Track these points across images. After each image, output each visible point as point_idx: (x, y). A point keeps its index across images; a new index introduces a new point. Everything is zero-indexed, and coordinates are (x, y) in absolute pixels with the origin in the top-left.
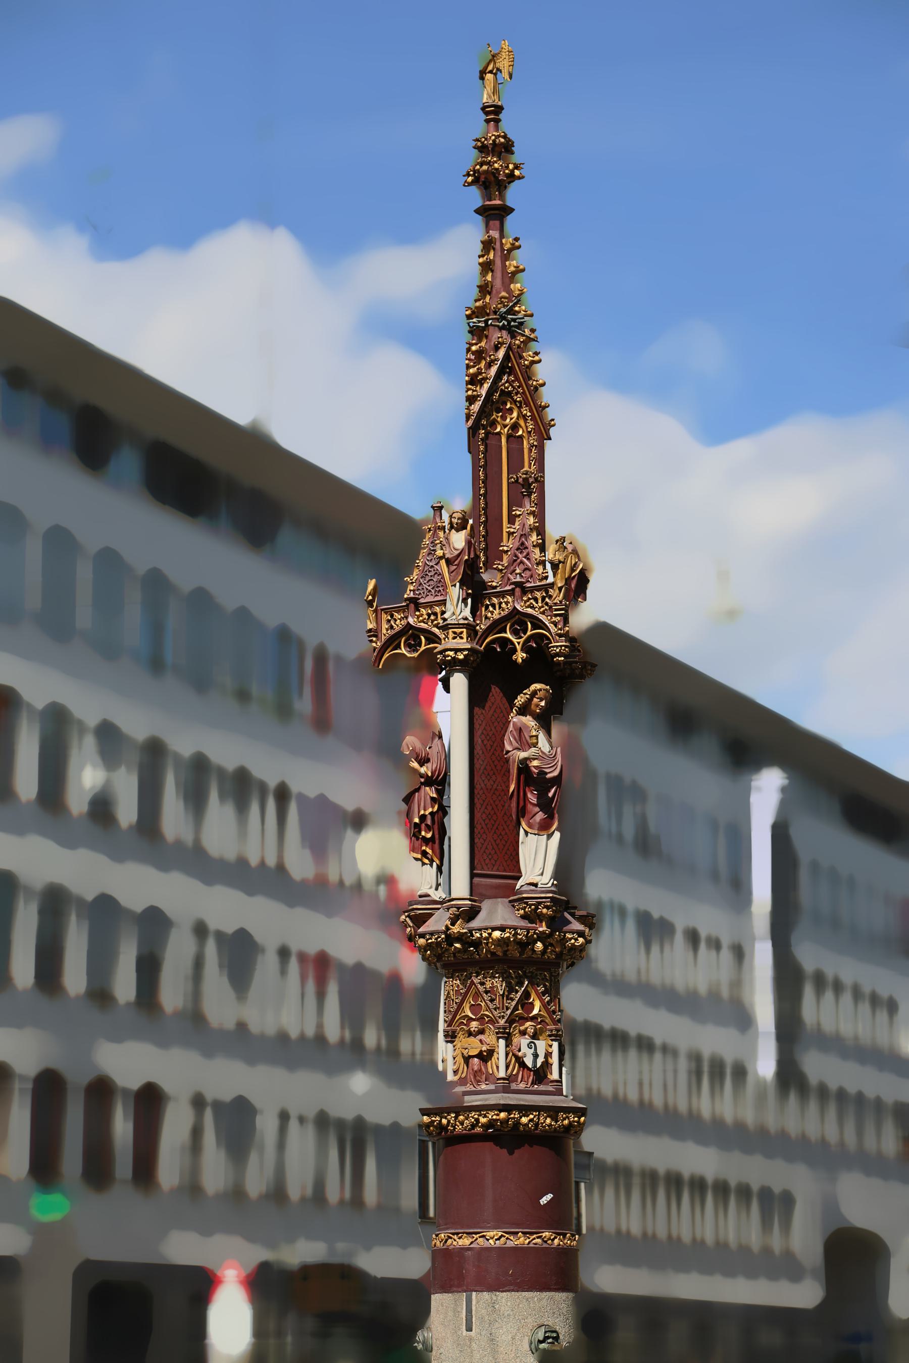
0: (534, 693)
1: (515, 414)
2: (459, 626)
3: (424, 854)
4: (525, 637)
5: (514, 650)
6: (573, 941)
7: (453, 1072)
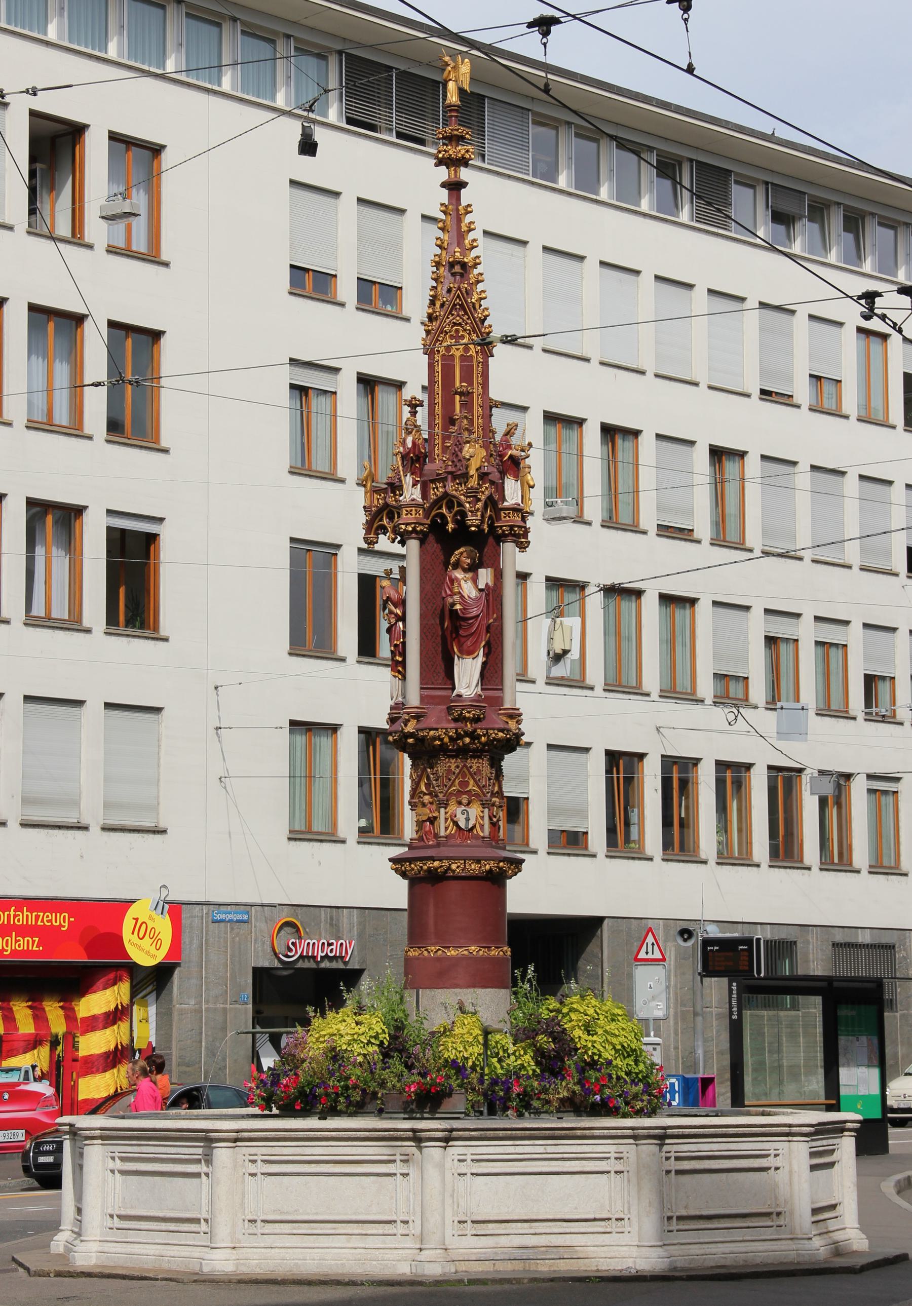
0: (462, 553)
6: (494, 735)
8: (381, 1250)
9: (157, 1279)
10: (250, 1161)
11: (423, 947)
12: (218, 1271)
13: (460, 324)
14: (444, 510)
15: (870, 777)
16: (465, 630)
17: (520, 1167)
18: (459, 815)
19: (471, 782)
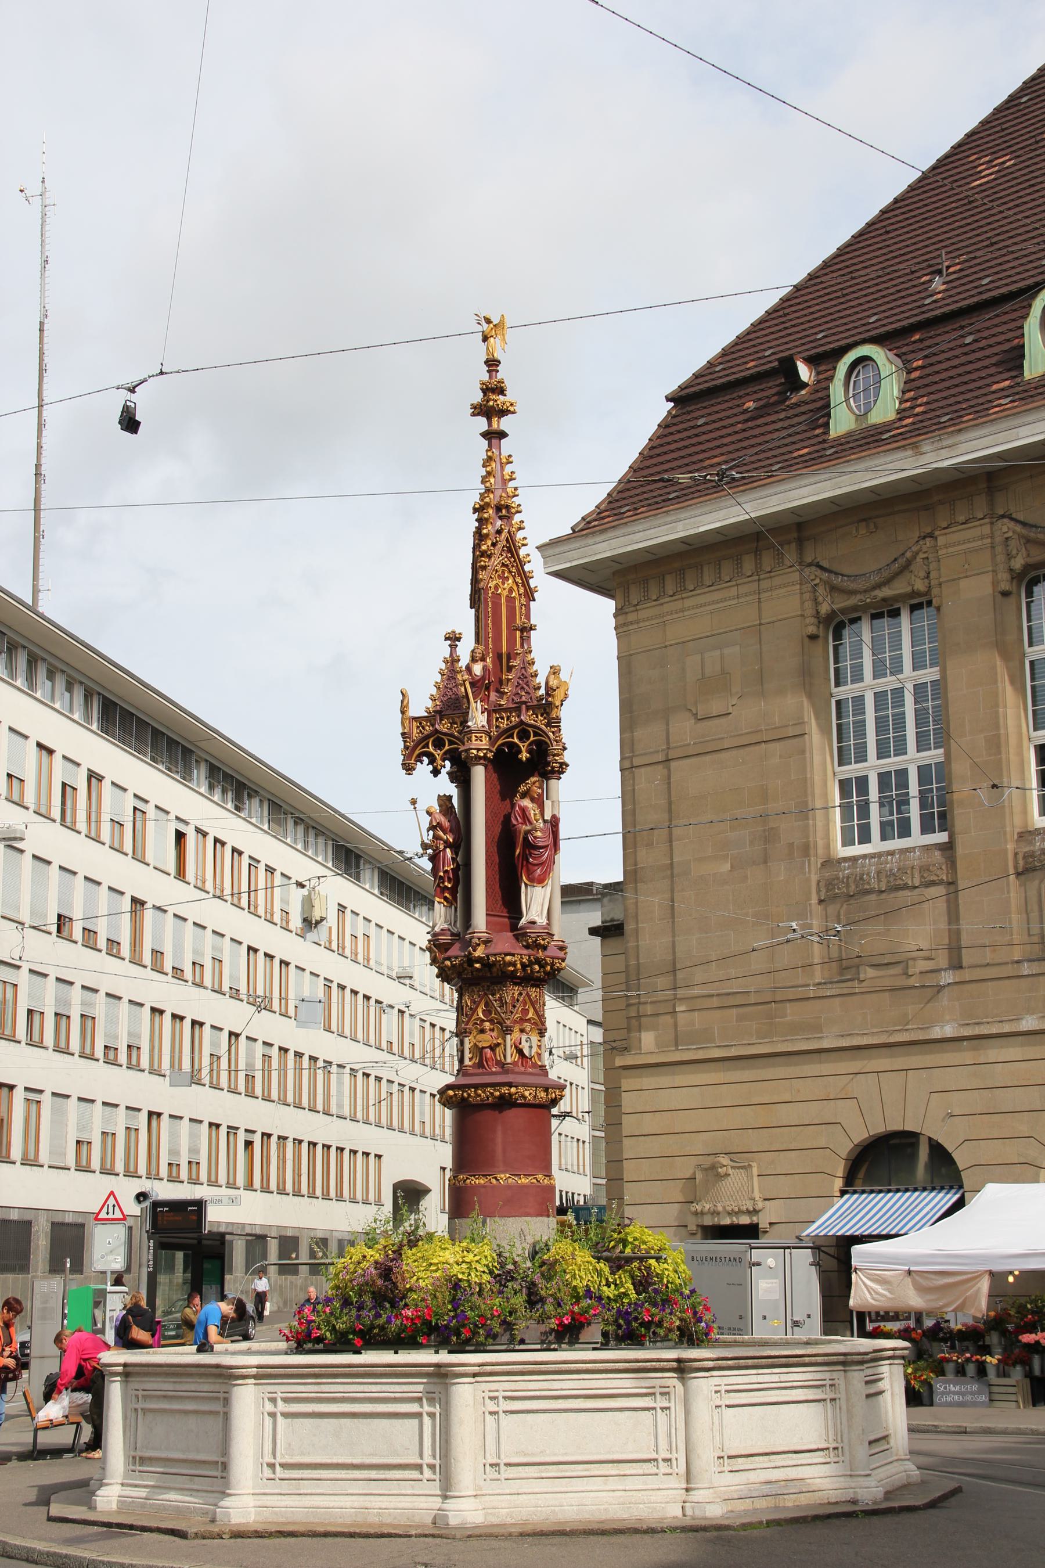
0: (534, 783)
1: (510, 581)
2: (479, 731)
5: (520, 752)
8: (642, 1492)
9: (410, 1536)
11: (489, 1175)
12: (470, 1523)
13: (506, 566)
14: (431, 749)
15: (27, 1089)
16: (534, 858)
17: (760, 1397)
19: (531, 1011)
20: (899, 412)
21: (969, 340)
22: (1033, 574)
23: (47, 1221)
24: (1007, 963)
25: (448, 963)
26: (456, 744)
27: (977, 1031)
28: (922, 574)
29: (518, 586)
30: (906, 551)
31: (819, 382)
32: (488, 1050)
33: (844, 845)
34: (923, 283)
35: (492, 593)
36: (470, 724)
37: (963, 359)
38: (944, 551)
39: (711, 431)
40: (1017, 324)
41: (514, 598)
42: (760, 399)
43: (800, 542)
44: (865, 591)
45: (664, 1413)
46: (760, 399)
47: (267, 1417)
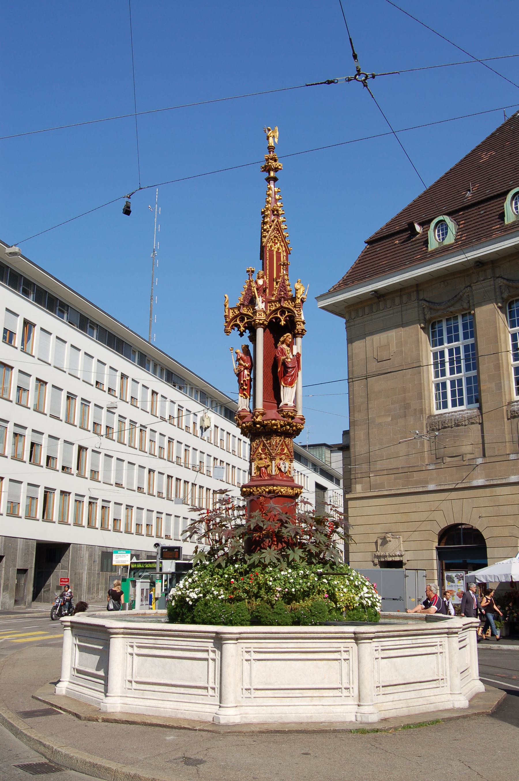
0: (288, 336)
1: (278, 244)
3: (244, 394)
4: (285, 316)
5: (281, 321)
6: (299, 426)
7: (26, 497)
9: (196, 730)
10: (246, 652)
13: (277, 237)
14: (238, 322)
18: (281, 465)
20: (455, 240)
21: (482, 212)
22: (511, 300)
23: (145, 555)
24: (504, 455)
25: (244, 425)
26: (250, 319)
27: (492, 483)
28: (467, 301)
29: (282, 247)
30: (460, 293)
31: (423, 232)
32: (263, 469)
33: (437, 409)
34: (463, 194)
35: (269, 249)
36: (256, 308)
37: (480, 219)
38: (475, 292)
39: (382, 253)
40: (501, 205)
41: (280, 253)
42: (401, 240)
43: (418, 291)
44: (444, 309)
45: (346, 662)
46: (401, 240)
47: (129, 656)
